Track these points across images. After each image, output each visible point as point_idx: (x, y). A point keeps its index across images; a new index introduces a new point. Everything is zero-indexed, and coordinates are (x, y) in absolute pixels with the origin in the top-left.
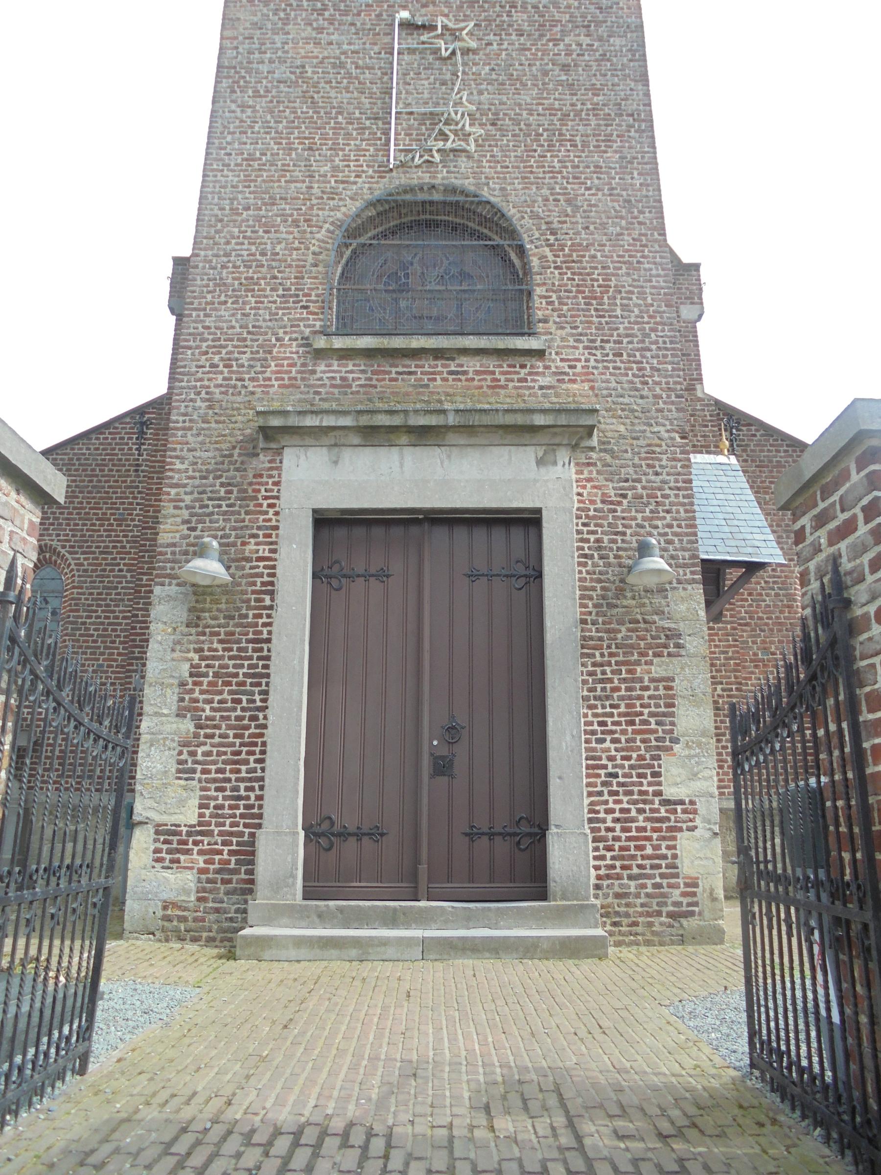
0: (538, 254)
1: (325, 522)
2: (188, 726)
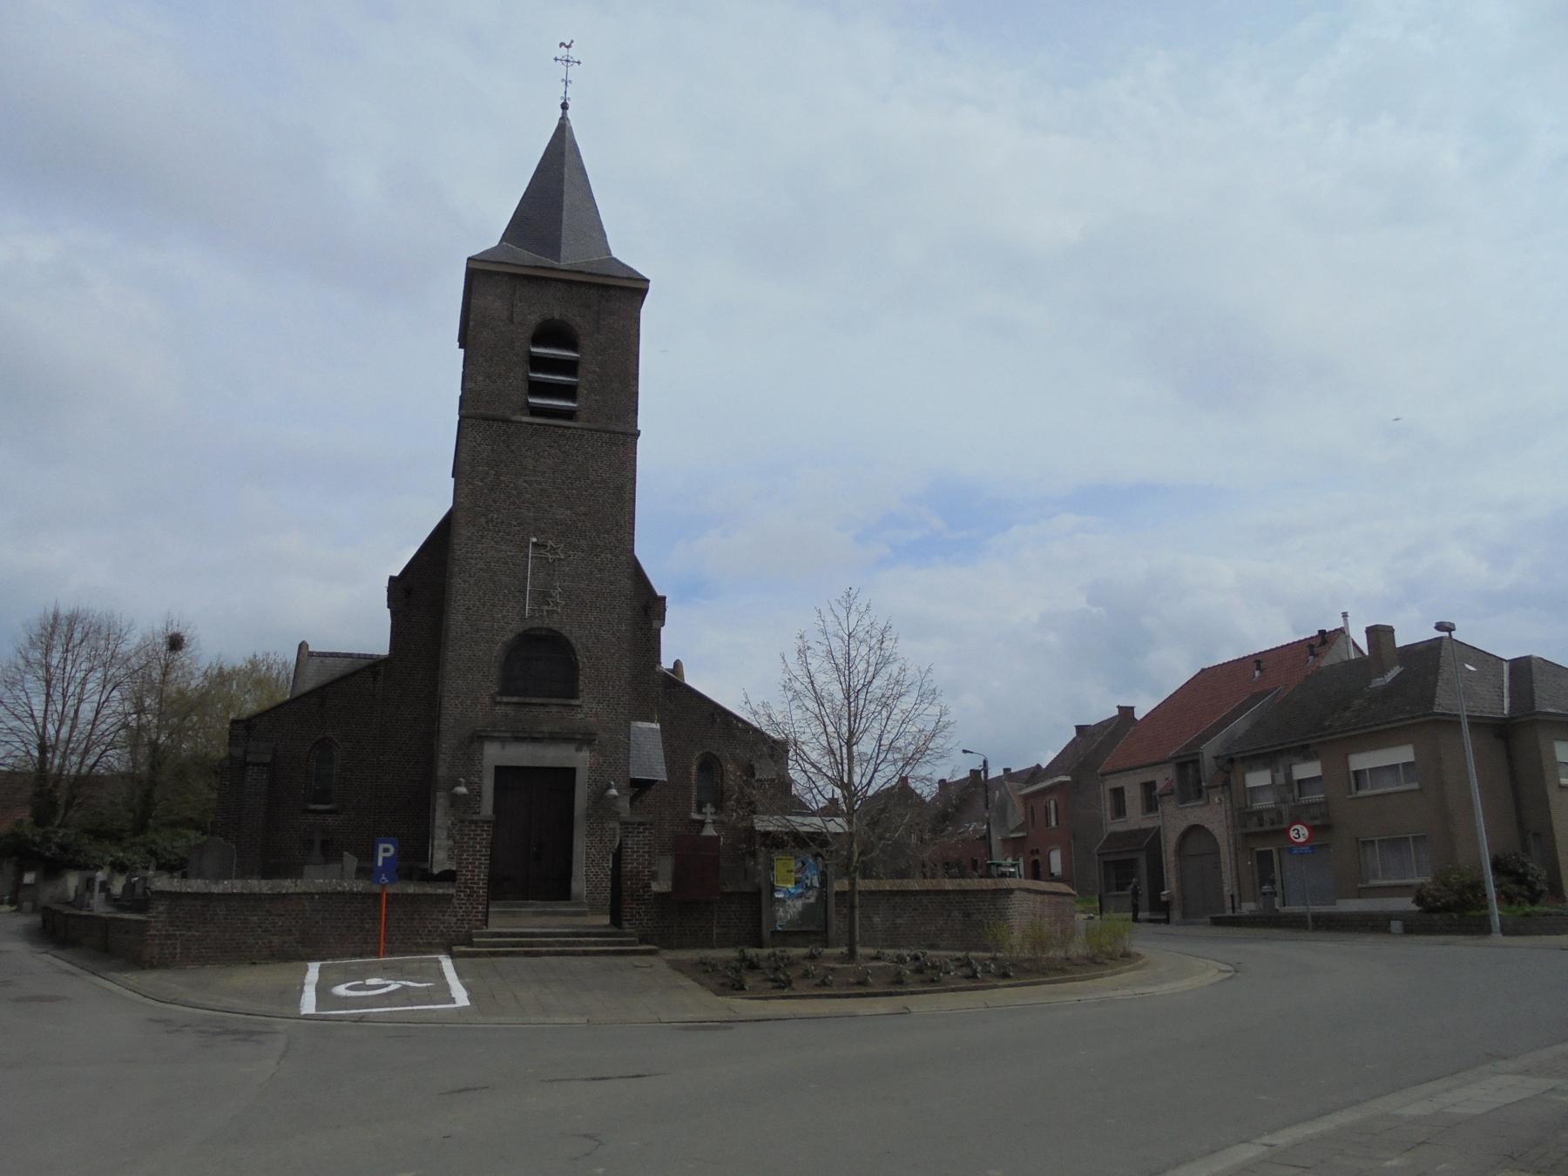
0: (582, 660)
1: (498, 769)
2: (451, 842)
